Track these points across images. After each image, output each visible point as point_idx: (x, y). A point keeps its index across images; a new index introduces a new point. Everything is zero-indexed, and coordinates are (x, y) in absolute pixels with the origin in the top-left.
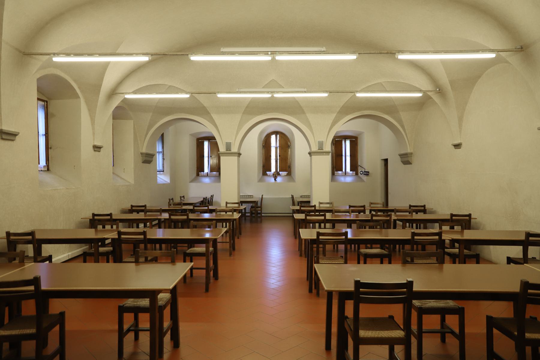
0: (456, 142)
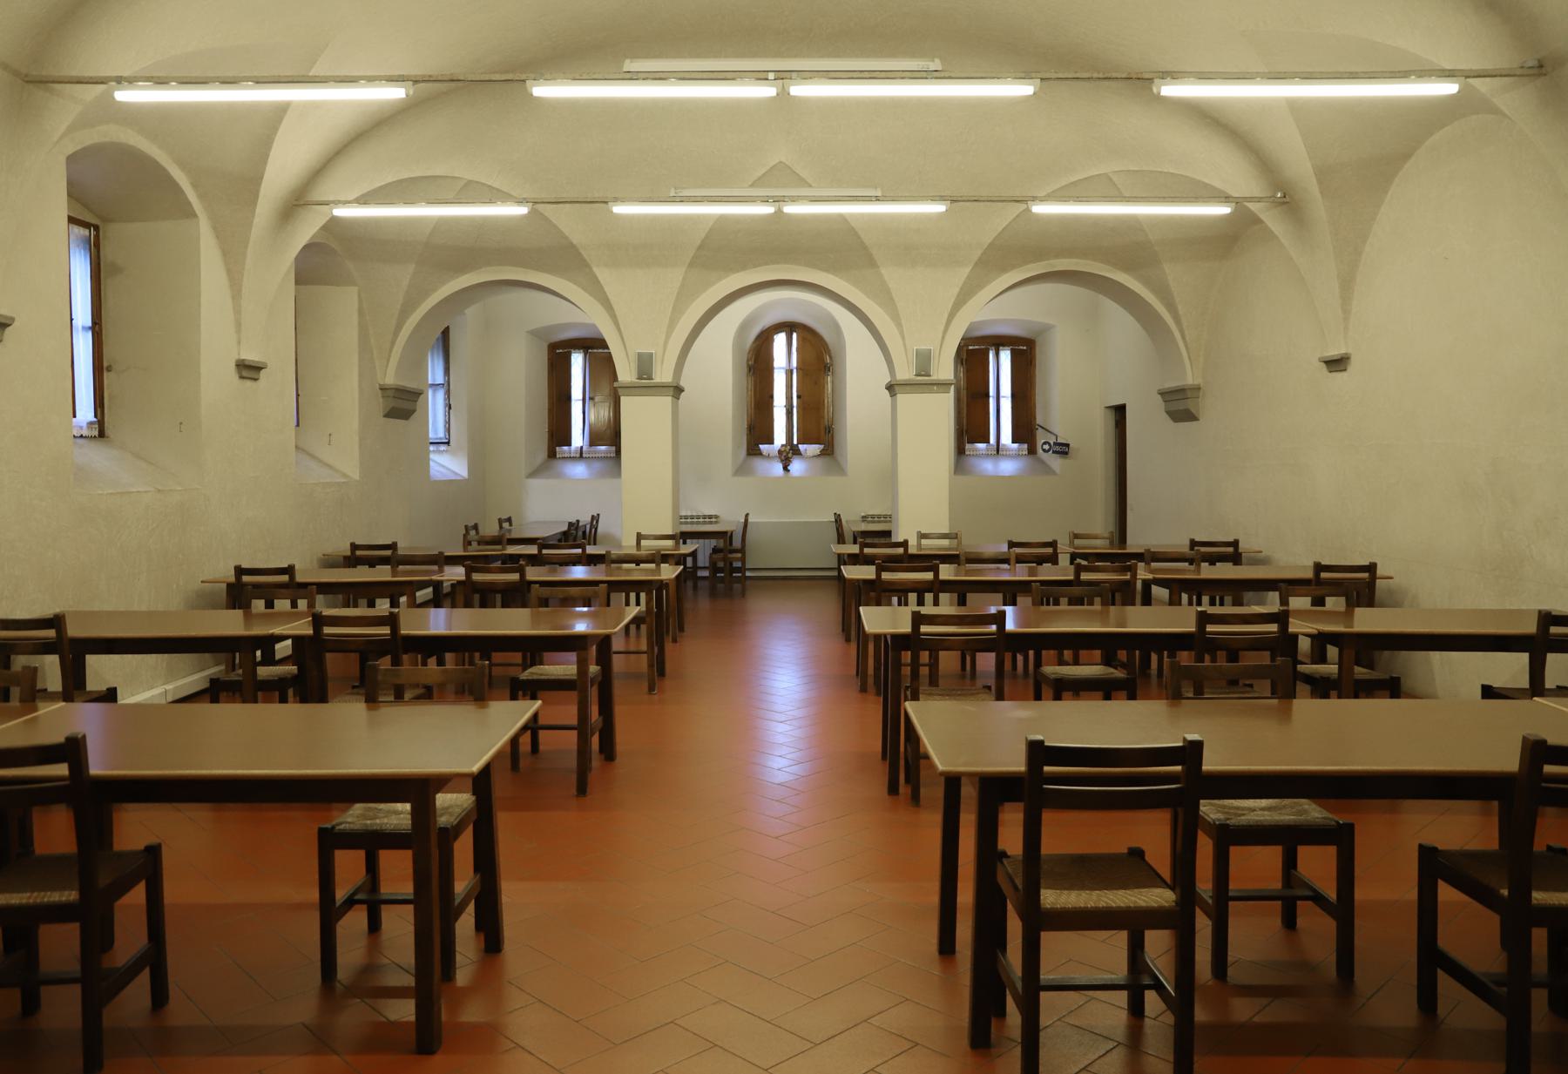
0: (1334, 352)
